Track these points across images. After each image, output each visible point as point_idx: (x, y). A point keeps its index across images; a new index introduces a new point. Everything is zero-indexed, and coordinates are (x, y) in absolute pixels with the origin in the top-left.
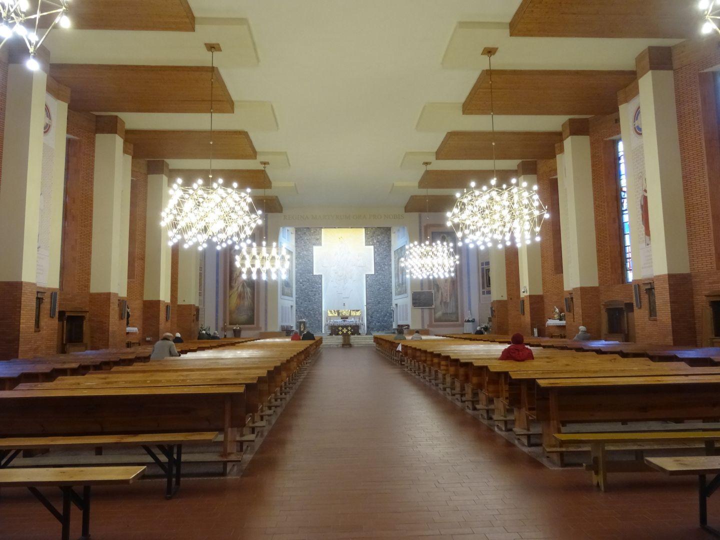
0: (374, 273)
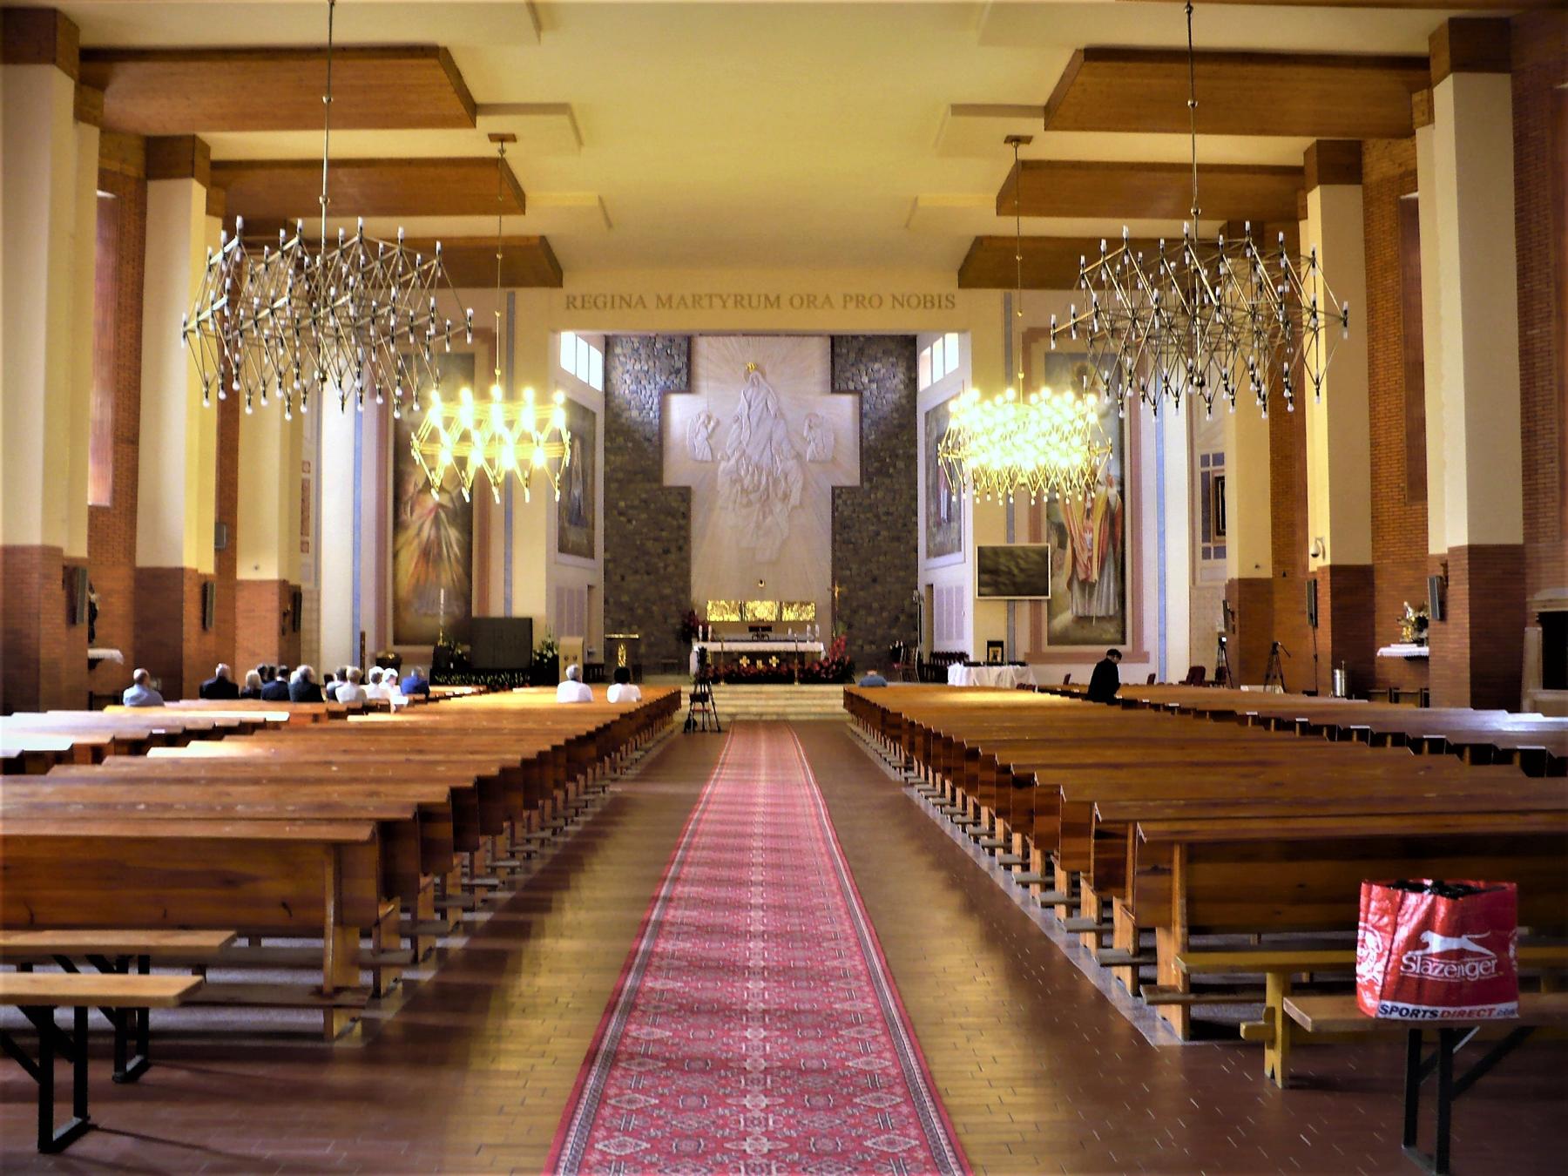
0: (857, 483)
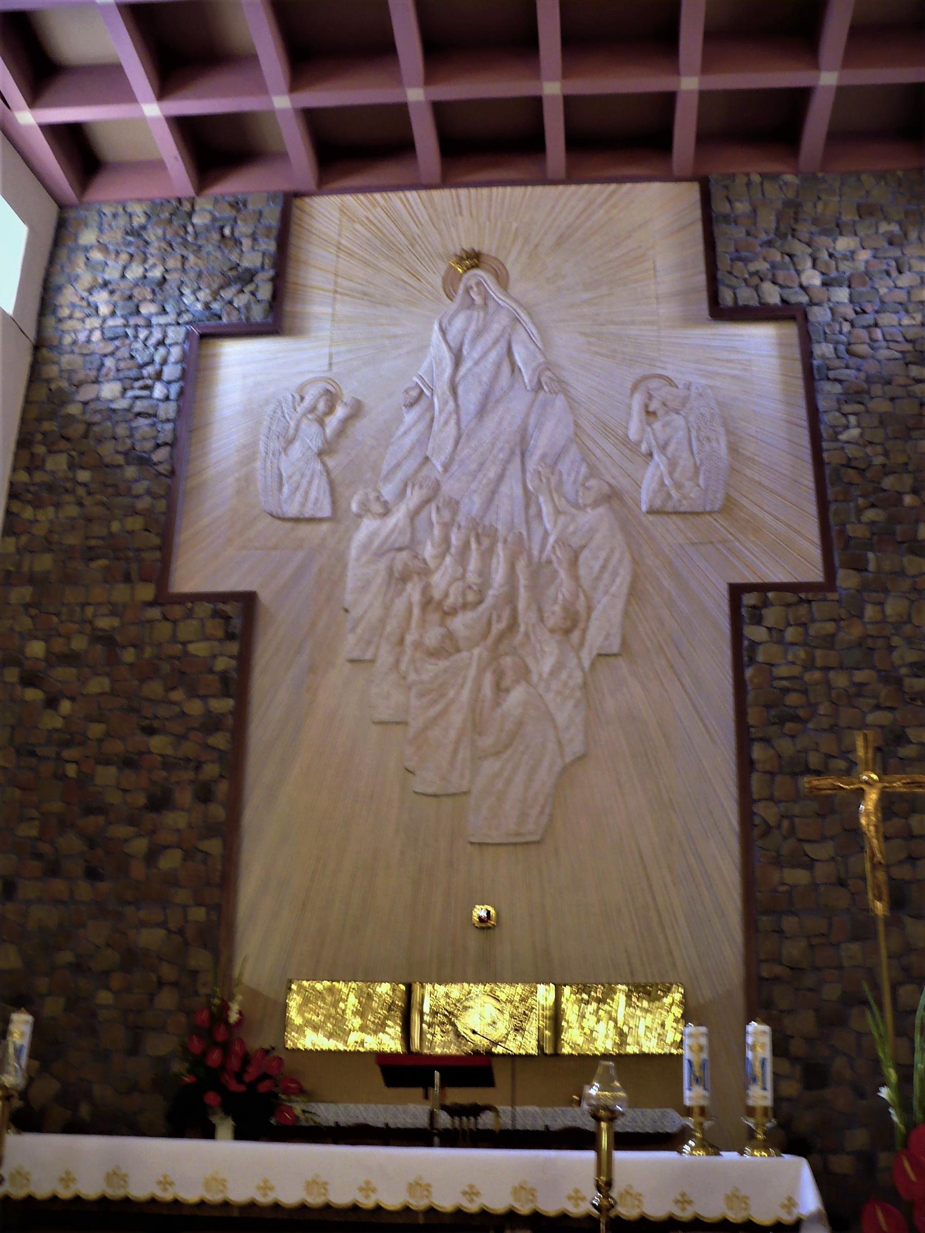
0: (816, 575)
